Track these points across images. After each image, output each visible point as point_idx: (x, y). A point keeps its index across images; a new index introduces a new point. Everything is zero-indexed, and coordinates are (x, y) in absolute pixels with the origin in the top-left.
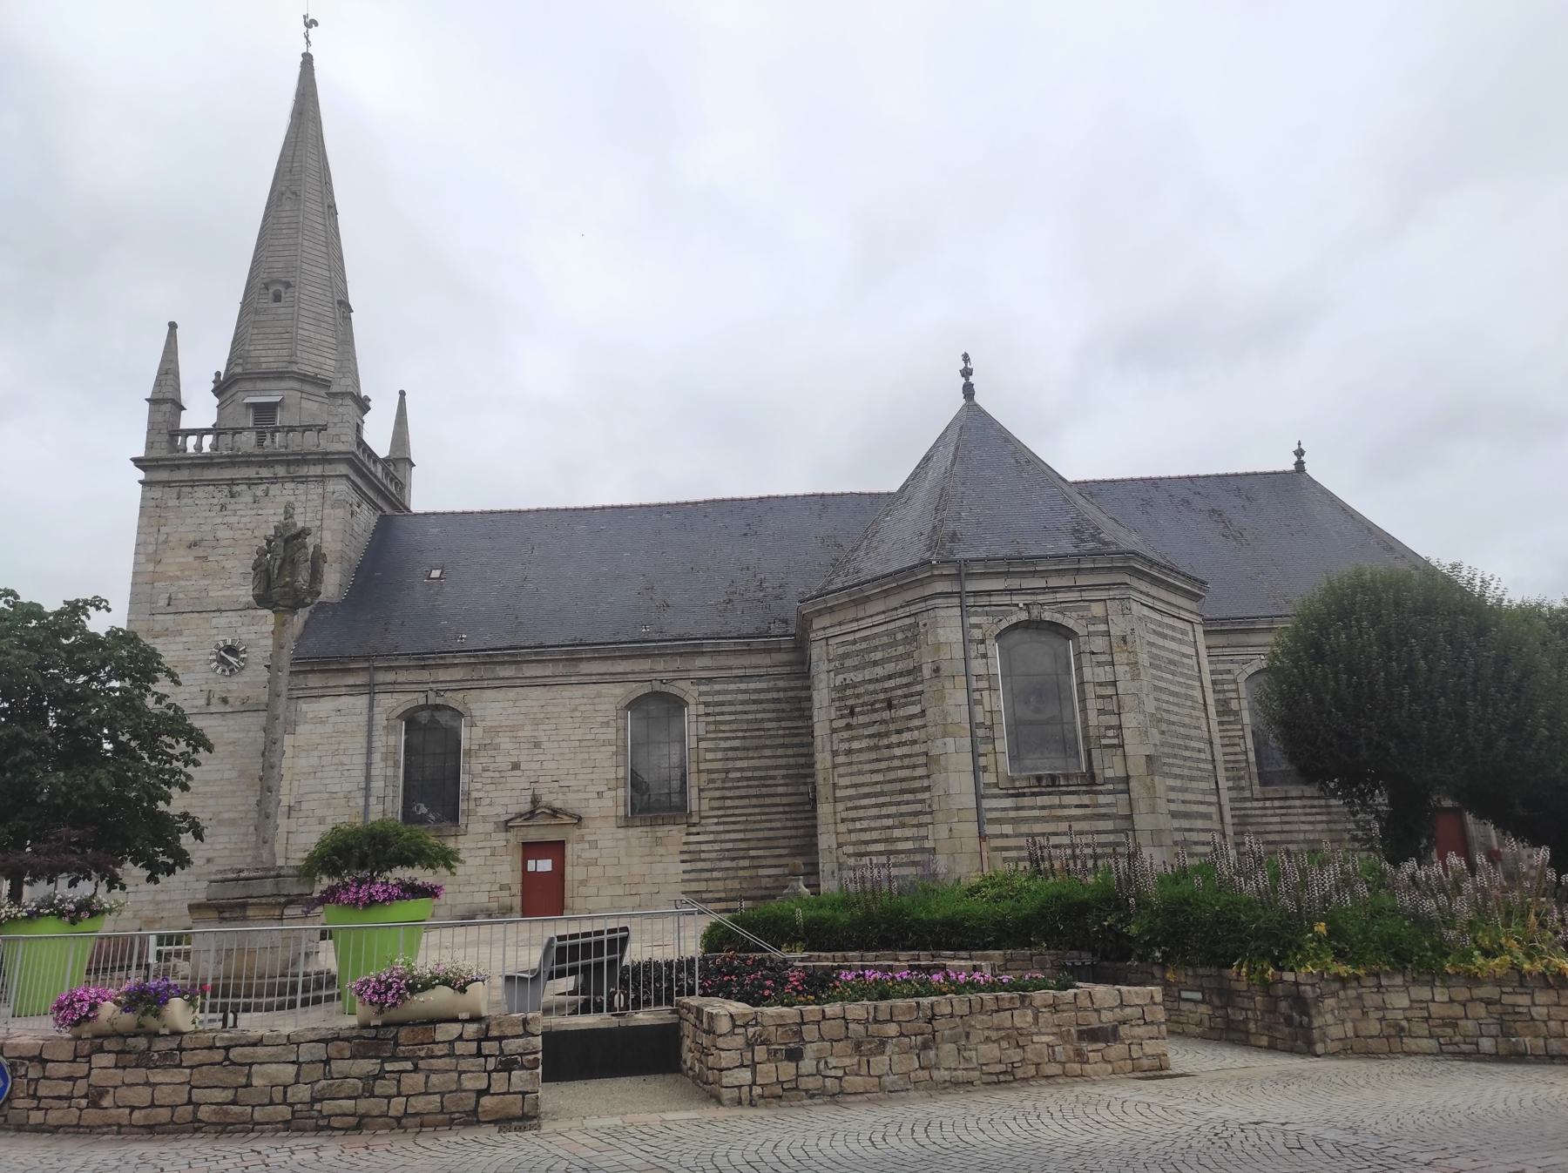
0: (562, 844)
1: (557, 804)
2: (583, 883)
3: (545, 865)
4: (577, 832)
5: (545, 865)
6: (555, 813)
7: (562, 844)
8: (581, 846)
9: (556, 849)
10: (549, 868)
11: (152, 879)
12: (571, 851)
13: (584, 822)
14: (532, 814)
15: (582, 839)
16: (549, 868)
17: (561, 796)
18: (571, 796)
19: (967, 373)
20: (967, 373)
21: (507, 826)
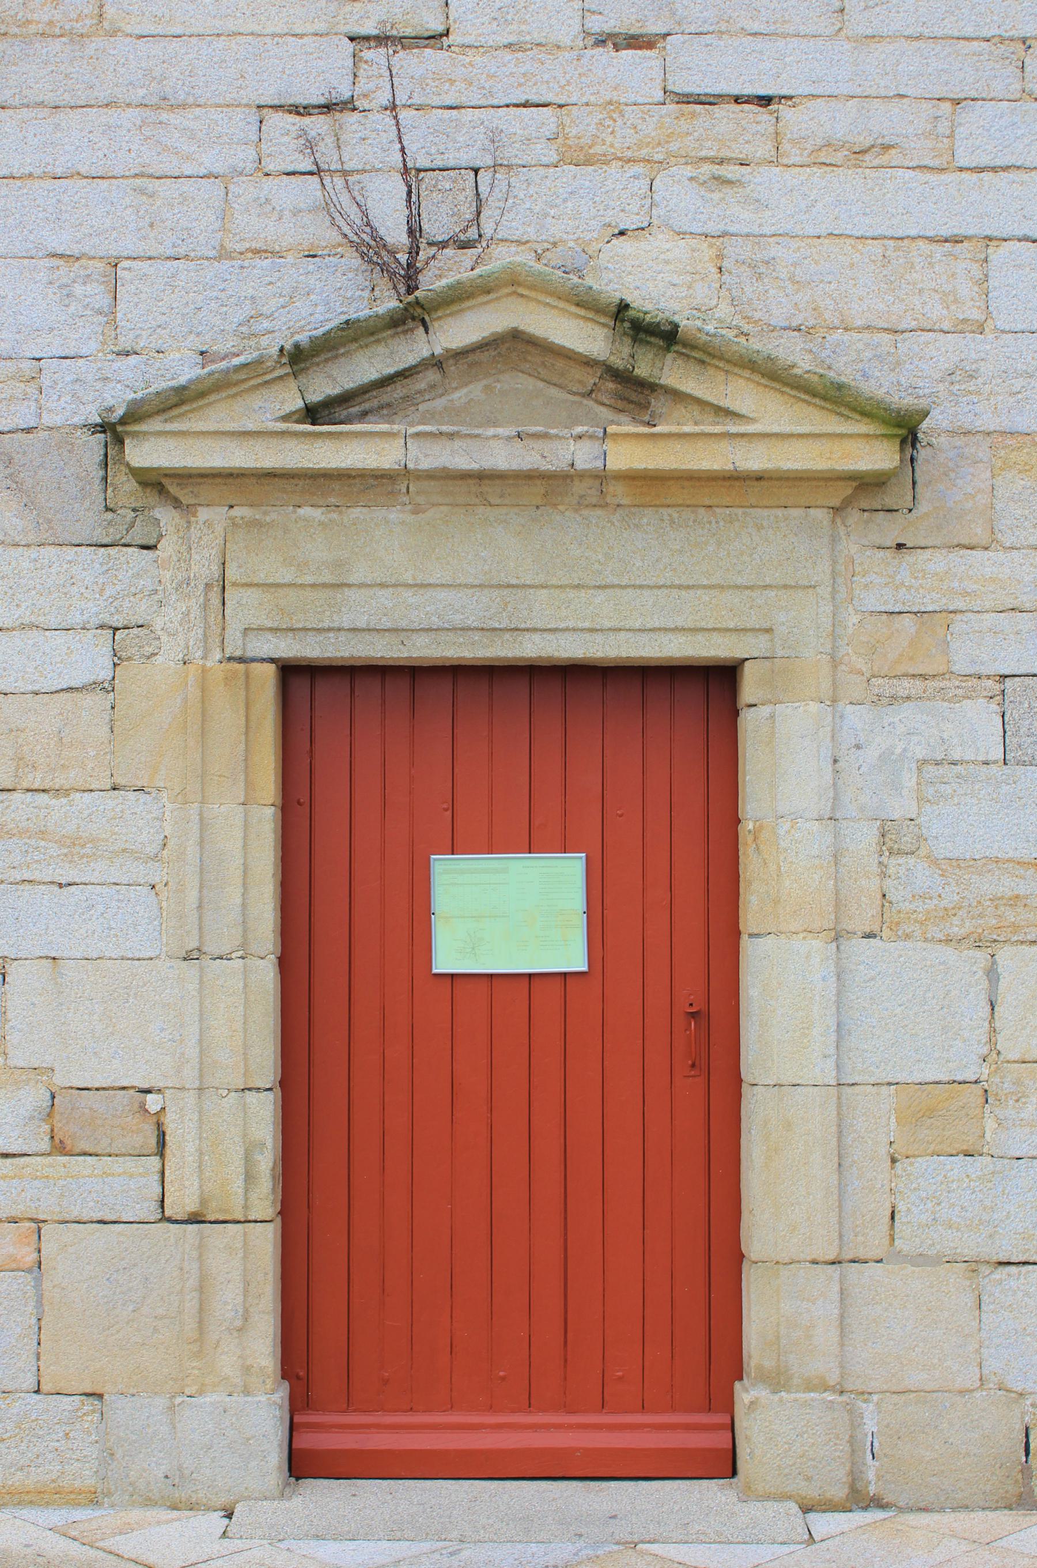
0: (702, 696)
1: (656, 279)
2: (947, 1114)
3: (508, 913)
4: (882, 584)
5: (508, 913)
6: (644, 355)
7: (702, 696)
8: (914, 728)
9: (649, 744)
10: (562, 948)
11: (657, 206)
12: (792, 769)
13: (957, 480)
14: (330, 379)
15: (914, 666)
16: (562, 948)
17: (679, 195)
18: (787, 199)
19: (815, 1262)
20: (815, 1262)
21: (135, 468)
